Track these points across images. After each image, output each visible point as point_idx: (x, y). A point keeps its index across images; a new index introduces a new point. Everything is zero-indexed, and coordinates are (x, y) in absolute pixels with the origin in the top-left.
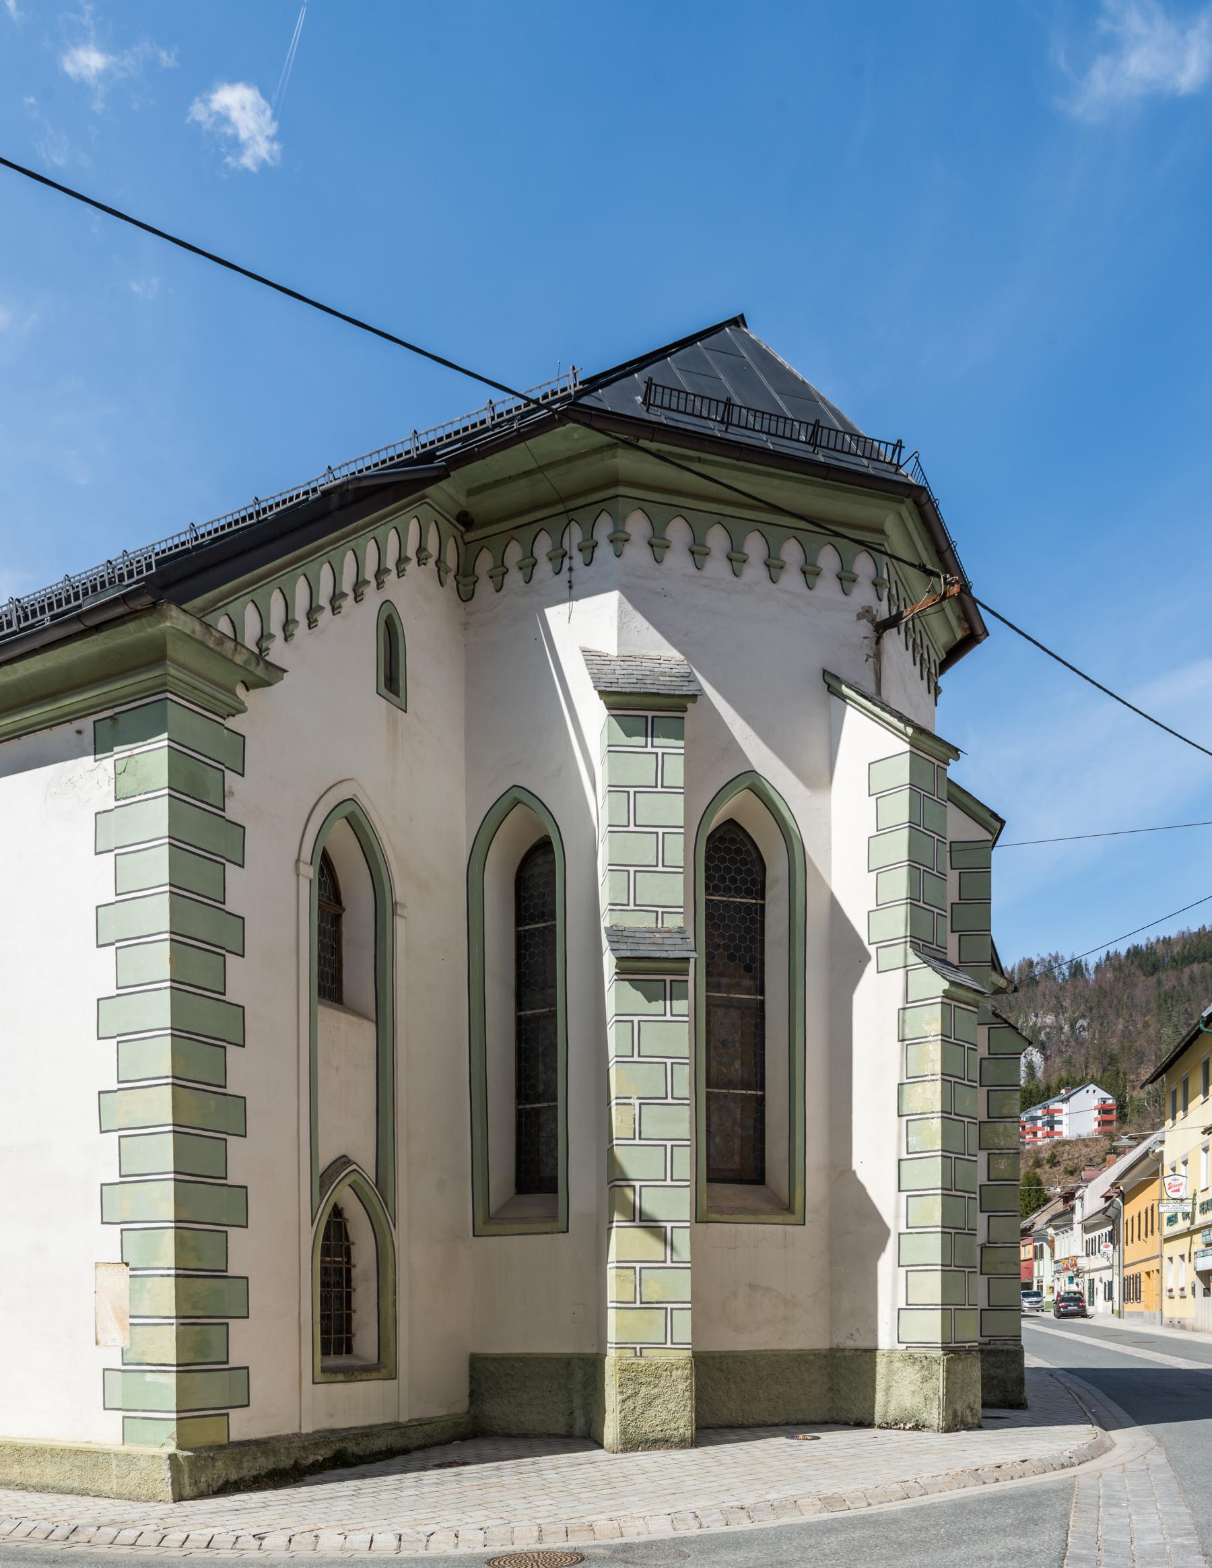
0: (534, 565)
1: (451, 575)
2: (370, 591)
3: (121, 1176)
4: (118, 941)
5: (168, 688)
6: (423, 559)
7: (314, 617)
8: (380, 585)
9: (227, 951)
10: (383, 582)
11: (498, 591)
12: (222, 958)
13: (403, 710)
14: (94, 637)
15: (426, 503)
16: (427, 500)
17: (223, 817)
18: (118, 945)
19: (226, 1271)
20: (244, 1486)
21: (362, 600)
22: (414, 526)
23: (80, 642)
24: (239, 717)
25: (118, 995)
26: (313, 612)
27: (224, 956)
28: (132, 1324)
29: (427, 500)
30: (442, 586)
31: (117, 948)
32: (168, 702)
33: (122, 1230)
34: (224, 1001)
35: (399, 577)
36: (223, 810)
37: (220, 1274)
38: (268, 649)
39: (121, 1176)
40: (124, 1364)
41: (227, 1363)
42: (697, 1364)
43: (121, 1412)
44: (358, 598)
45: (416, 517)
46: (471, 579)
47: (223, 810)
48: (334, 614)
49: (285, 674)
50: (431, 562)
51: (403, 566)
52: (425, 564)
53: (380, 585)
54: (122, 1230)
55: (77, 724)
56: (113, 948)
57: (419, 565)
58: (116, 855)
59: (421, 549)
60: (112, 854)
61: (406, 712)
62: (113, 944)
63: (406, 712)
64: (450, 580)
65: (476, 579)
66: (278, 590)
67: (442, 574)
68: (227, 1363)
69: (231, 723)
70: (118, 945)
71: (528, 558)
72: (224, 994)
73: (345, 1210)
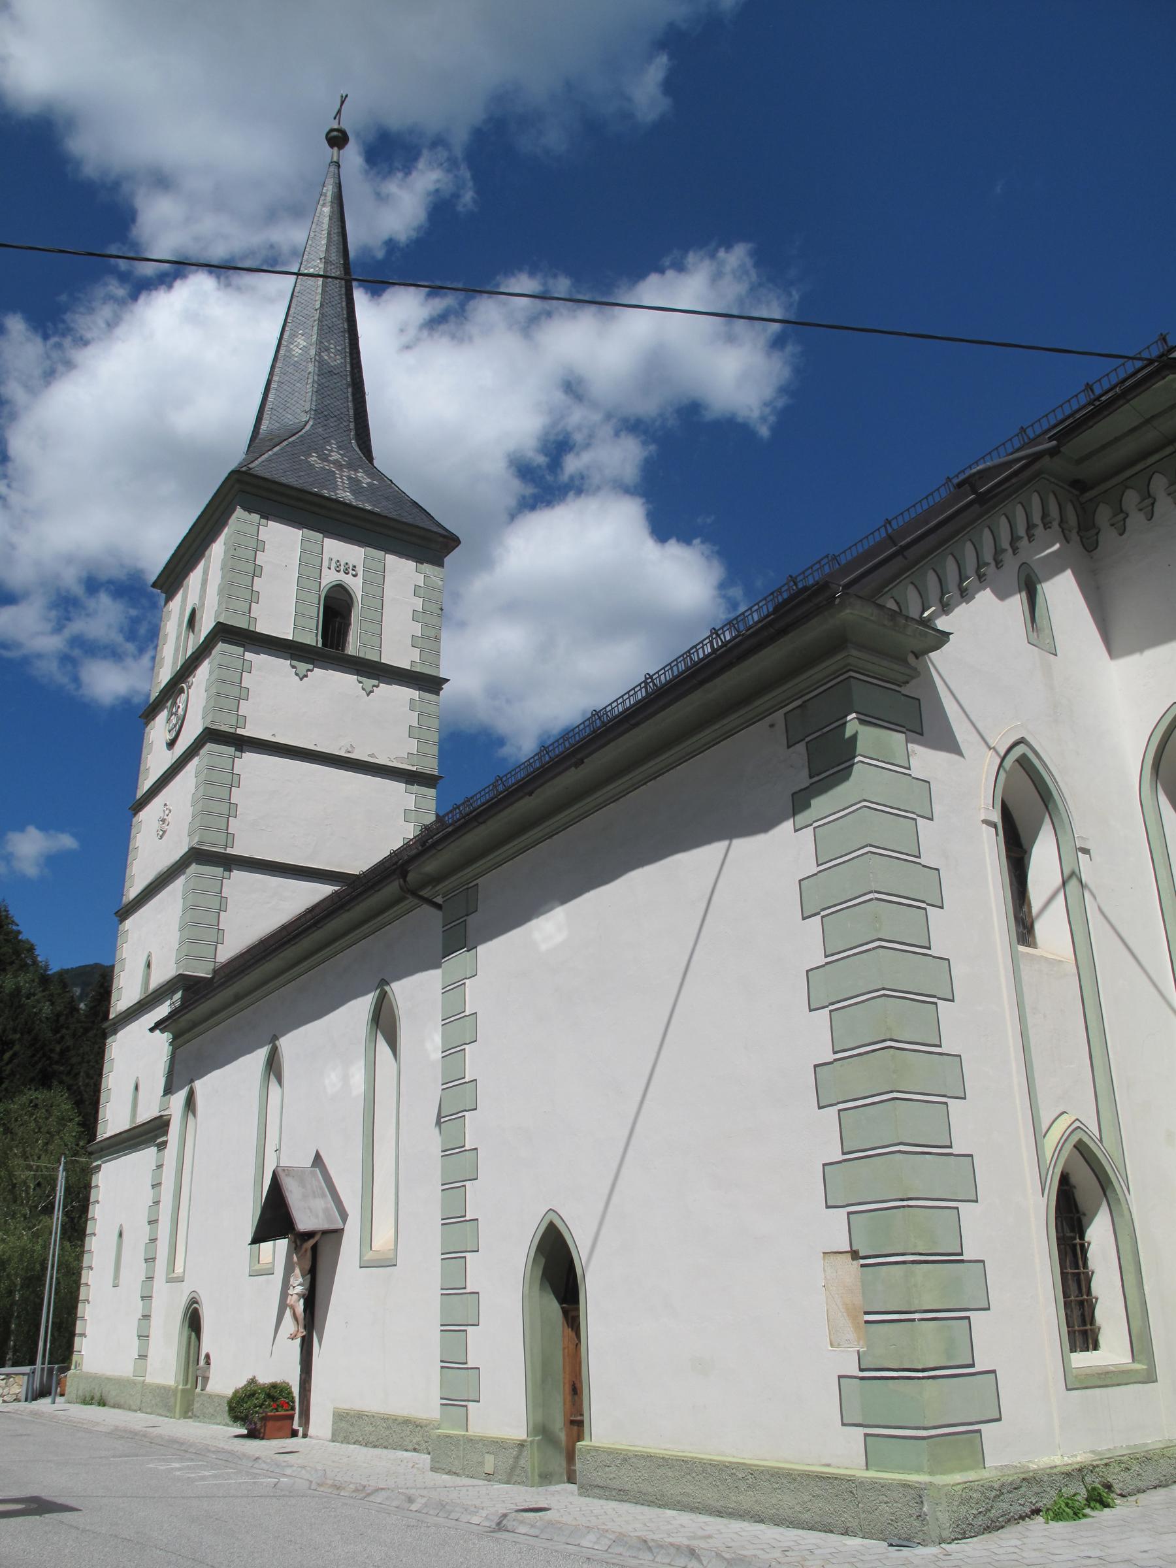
0: (1153, 504)
1: (1075, 531)
2: (1008, 557)
3: (844, 1153)
4: (823, 910)
5: (852, 668)
6: (1047, 524)
7: (1000, 558)
8: (1015, 551)
9: (928, 904)
10: (1017, 548)
11: (1121, 535)
12: (924, 911)
13: (1053, 654)
14: (782, 640)
15: (1043, 478)
16: (1043, 476)
17: (910, 775)
18: (823, 913)
19: (961, 1254)
20: (23, 1293)
21: (1002, 566)
22: (1036, 500)
23: (771, 647)
24: (913, 683)
25: (827, 963)
26: (1014, 540)
27: (925, 909)
28: (867, 1322)
29: (1043, 476)
30: (1068, 542)
31: (822, 917)
32: (852, 679)
33: (849, 1214)
34: (930, 955)
35: (1030, 542)
36: (909, 769)
37: (954, 1258)
38: (1001, 561)
39: (844, 1153)
40: (861, 1370)
41: (972, 1366)
42: (38, 1301)
43: (861, 1428)
44: (998, 564)
45: (1035, 491)
46: (1094, 531)
47: (909, 769)
48: (981, 583)
49: (951, 636)
50: (1055, 525)
51: (1032, 531)
52: (1050, 527)
53: (1015, 551)
54: (849, 1214)
55: (768, 720)
56: (819, 917)
57: (1045, 529)
58: (814, 828)
59: (1045, 515)
60: (812, 827)
61: (1056, 655)
62: (818, 914)
63: (1056, 655)
64: (1075, 537)
65: (1097, 530)
66: (932, 570)
67: (1067, 532)
68: (972, 1366)
69: (905, 690)
70: (823, 913)
71: (1147, 499)
72: (929, 948)
73: (1071, 1176)
